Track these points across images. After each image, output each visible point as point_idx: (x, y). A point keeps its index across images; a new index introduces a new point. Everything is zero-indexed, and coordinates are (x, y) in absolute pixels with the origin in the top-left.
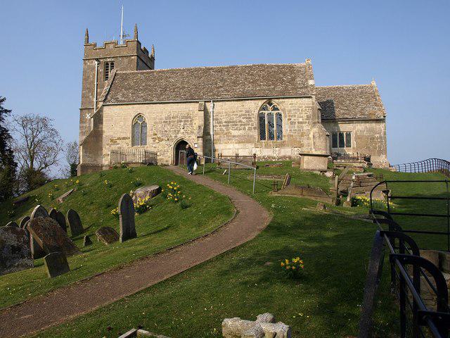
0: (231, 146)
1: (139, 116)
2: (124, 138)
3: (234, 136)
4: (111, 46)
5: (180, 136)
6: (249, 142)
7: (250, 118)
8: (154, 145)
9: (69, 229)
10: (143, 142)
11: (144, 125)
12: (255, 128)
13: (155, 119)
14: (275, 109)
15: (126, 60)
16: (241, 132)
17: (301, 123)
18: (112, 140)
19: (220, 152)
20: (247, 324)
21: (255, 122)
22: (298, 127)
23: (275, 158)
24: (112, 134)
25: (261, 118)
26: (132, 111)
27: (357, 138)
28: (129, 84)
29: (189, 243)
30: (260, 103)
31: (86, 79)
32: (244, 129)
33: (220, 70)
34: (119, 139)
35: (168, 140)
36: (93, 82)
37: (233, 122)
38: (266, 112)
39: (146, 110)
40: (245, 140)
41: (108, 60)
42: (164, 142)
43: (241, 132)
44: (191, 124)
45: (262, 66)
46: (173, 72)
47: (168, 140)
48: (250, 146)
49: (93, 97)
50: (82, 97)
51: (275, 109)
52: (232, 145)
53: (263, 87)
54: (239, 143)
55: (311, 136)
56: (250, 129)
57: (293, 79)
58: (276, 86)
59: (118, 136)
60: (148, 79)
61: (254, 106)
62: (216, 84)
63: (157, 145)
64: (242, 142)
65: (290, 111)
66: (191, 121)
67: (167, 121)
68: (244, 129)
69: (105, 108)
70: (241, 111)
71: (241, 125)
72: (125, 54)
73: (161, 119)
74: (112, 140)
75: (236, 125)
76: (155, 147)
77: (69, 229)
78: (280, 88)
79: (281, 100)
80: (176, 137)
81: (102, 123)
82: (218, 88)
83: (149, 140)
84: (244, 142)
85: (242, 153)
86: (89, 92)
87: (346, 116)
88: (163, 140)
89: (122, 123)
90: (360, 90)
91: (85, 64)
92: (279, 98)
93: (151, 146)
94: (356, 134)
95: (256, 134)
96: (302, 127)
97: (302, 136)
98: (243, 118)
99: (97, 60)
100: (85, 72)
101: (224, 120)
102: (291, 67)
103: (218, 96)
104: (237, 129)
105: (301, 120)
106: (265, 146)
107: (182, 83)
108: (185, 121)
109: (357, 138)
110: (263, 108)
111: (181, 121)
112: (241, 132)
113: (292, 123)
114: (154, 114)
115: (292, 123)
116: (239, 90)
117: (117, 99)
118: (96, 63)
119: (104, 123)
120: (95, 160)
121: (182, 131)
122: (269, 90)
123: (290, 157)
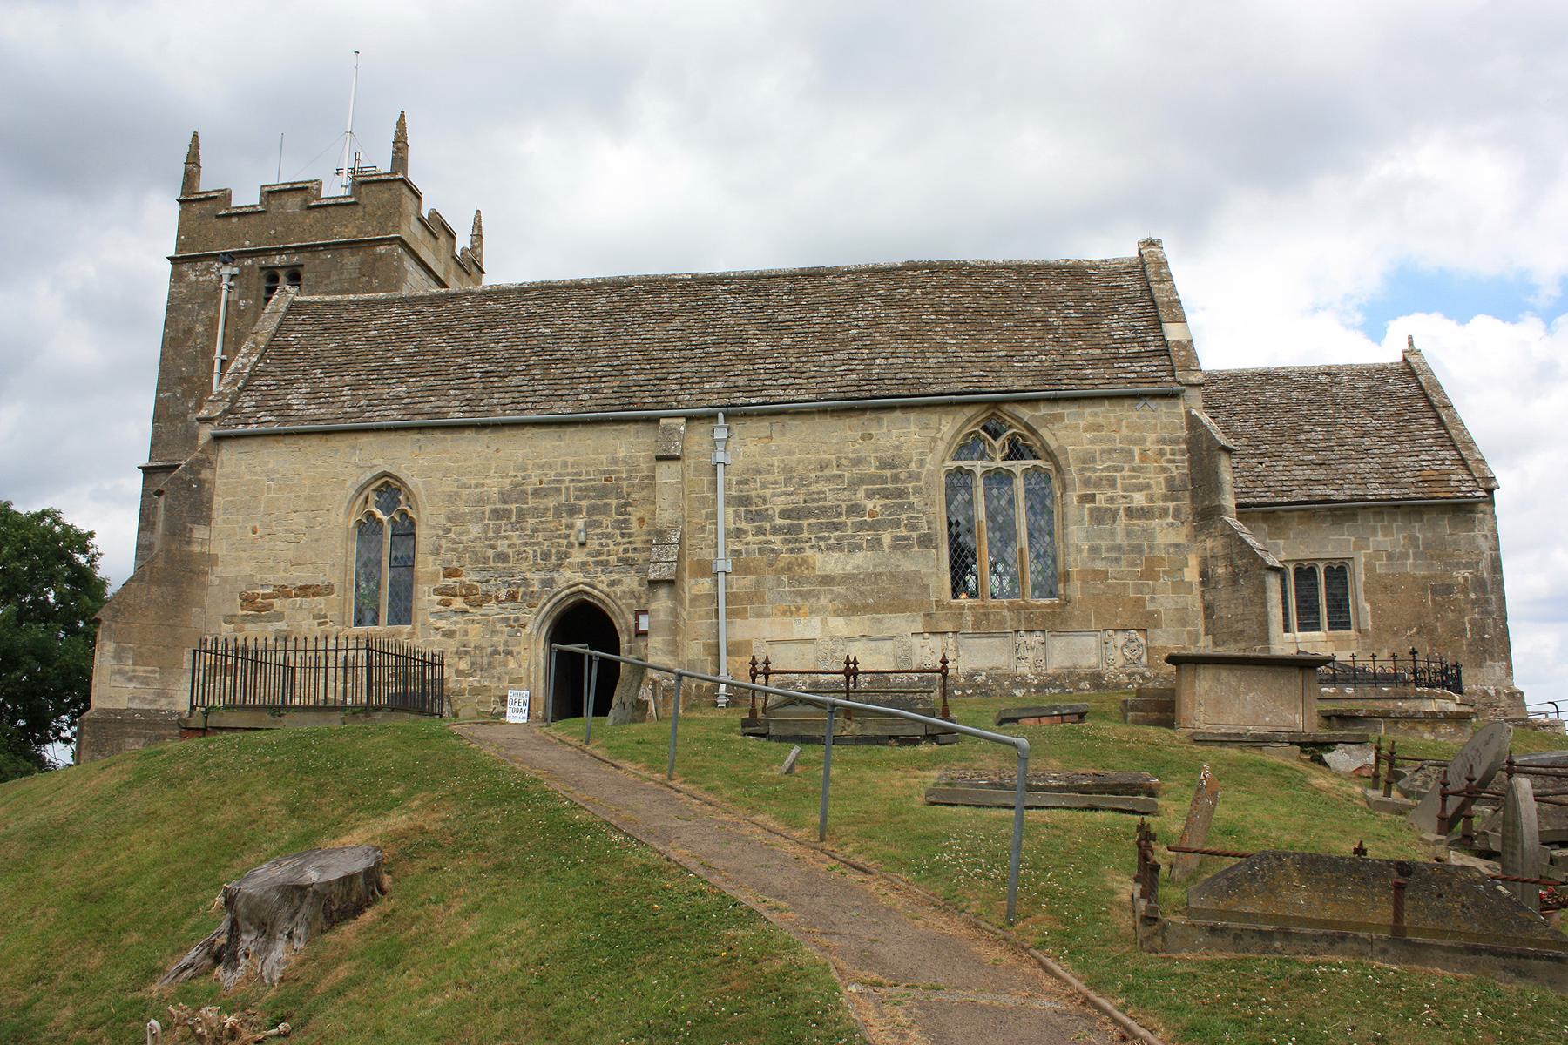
0: (809, 627)
1: (389, 488)
2: (305, 591)
3: (827, 580)
4: (293, 203)
5: (569, 579)
6: (898, 606)
7: (901, 493)
8: (443, 624)
10: (402, 613)
11: (406, 531)
13: (452, 498)
15: (351, 260)
16: (860, 560)
17: (1144, 513)
18: (249, 600)
20: (460, 673)
22: (1129, 534)
23: (1024, 684)
24: (247, 568)
26: (348, 466)
27: (1379, 586)
28: (346, 350)
30: (949, 426)
32: (876, 544)
35: (512, 597)
36: (207, 352)
37: (824, 511)
39: (411, 460)
40: (873, 598)
41: (277, 260)
42: (492, 608)
43: (860, 560)
44: (623, 525)
47: (512, 597)
48: (903, 625)
50: (157, 417)
52: (816, 621)
53: (951, 358)
55: (1191, 574)
59: (281, 577)
60: (428, 327)
61: (924, 444)
62: (741, 342)
63: (457, 623)
64: (866, 609)
65: (1087, 460)
66: (623, 509)
67: (510, 509)
68: (876, 544)
70: (857, 462)
71: (860, 527)
72: (349, 233)
73: (481, 501)
74: (249, 600)
75: (836, 527)
76: (449, 634)
79: (1044, 410)
80: (548, 583)
81: (207, 520)
82: (751, 360)
83: (425, 599)
85: (871, 658)
86: (186, 395)
87: (1320, 491)
88: (487, 597)
89: (298, 521)
90: (1362, 385)
92: (1037, 400)
93: (429, 630)
94: (1370, 568)
95: (935, 567)
96: (1148, 533)
97: (1150, 573)
98: (870, 495)
101: (779, 504)
103: (749, 392)
104: (839, 546)
105: (1139, 500)
106: (977, 625)
107: (586, 339)
108: (592, 510)
109: (1379, 586)
111: (573, 511)
112: (859, 558)
113: (1099, 516)
114: (451, 477)
115: (1099, 516)
116: (845, 370)
117: (283, 412)
119: (218, 516)
120: (162, 694)
122: (987, 366)
123: (1096, 679)
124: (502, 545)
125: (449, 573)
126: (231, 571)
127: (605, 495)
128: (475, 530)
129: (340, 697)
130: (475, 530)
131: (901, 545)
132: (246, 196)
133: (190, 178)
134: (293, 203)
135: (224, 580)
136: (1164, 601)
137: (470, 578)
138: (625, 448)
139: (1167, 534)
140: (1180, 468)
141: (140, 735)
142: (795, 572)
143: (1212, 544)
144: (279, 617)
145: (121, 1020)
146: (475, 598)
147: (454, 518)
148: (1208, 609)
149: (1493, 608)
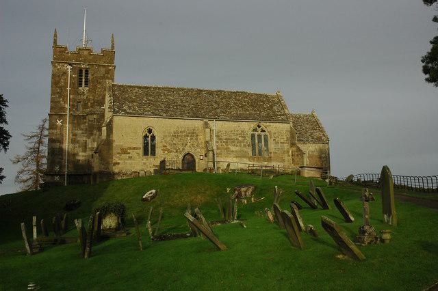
2: (134, 148)
3: (233, 151)
5: (187, 150)
9: (34, 223)
11: (153, 138)
12: (248, 145)
13: (164, 132)
14: (263, 131)
18: (122, 149)
19: (26, 143)
21: (249, 140)
25: (253, 136)
29: (212, 241)
31: (55, 83)
33: (211, 93)
34: (130, 148)
35: (177, 152)
38: (256, 133)
40: (241, 155)
44: (197, 139)
45: (244, 93)
46: (169, 89)
47: (177, 152)
49: (66, 102)
50: (51, 102)
51: (263, 131)
54: (237, 157)
55: (290, 153)
56: (245, 146)
57: (271, 107)
58: (261, 112)
61: (247, 127)
67: (175, 135)
69: (116, 119)
77: (34, 223)
78: (264, 114)
80: (183, 149)
83: (159, 151)
84: (241, 157)
91: (55, 67)
95: (249, 151)
99: (70, 65)
100: (54, 76)
102: (266, 96)
105: (282, 141)
110: (255, 130)
111: (188, 136)
115: (276, 143)
118: (69, 67)
121: (189, 144)
124: (174, 142)
125: (164, 146)
126: (117, 144)
127: (193, 134)
128: (169, 139)
129: (430, 185)
130: (169, 139)
131: (245, 146)
132: (72, 49)
133: (55, 42)
134: (86, 53)
135: (117, 145)
136: (286, 158)
137: (168, 147)
138: (197, 124)
139: (286, 147)
140: (289, 136)
141: (131, 174)
142: (227, 149)
143: (294, 149)
144: (129, 153)
145: (157, 222)
146: (169, 151)
147: (166, 136)
148: (293, 160)
149: (140, 91)
